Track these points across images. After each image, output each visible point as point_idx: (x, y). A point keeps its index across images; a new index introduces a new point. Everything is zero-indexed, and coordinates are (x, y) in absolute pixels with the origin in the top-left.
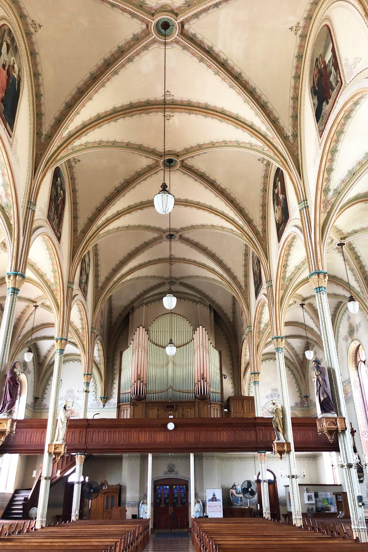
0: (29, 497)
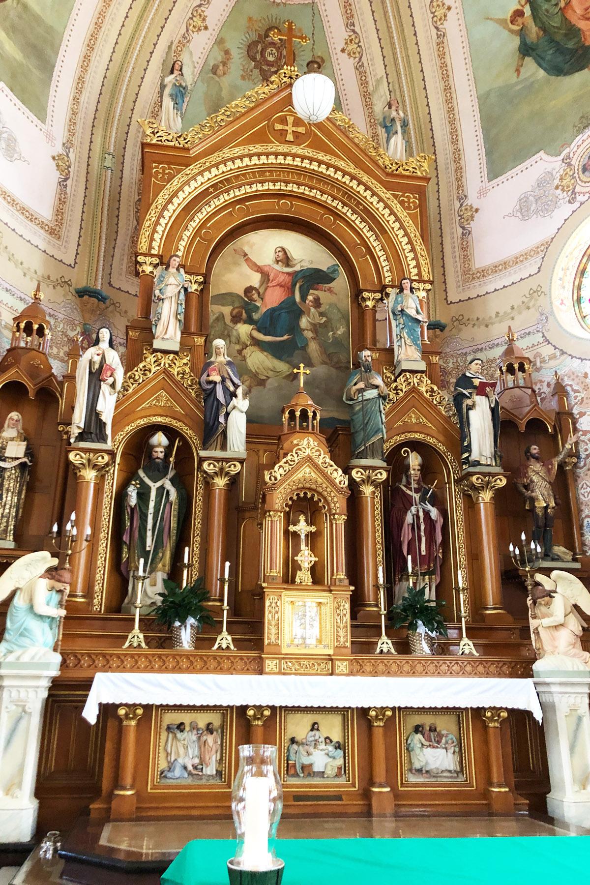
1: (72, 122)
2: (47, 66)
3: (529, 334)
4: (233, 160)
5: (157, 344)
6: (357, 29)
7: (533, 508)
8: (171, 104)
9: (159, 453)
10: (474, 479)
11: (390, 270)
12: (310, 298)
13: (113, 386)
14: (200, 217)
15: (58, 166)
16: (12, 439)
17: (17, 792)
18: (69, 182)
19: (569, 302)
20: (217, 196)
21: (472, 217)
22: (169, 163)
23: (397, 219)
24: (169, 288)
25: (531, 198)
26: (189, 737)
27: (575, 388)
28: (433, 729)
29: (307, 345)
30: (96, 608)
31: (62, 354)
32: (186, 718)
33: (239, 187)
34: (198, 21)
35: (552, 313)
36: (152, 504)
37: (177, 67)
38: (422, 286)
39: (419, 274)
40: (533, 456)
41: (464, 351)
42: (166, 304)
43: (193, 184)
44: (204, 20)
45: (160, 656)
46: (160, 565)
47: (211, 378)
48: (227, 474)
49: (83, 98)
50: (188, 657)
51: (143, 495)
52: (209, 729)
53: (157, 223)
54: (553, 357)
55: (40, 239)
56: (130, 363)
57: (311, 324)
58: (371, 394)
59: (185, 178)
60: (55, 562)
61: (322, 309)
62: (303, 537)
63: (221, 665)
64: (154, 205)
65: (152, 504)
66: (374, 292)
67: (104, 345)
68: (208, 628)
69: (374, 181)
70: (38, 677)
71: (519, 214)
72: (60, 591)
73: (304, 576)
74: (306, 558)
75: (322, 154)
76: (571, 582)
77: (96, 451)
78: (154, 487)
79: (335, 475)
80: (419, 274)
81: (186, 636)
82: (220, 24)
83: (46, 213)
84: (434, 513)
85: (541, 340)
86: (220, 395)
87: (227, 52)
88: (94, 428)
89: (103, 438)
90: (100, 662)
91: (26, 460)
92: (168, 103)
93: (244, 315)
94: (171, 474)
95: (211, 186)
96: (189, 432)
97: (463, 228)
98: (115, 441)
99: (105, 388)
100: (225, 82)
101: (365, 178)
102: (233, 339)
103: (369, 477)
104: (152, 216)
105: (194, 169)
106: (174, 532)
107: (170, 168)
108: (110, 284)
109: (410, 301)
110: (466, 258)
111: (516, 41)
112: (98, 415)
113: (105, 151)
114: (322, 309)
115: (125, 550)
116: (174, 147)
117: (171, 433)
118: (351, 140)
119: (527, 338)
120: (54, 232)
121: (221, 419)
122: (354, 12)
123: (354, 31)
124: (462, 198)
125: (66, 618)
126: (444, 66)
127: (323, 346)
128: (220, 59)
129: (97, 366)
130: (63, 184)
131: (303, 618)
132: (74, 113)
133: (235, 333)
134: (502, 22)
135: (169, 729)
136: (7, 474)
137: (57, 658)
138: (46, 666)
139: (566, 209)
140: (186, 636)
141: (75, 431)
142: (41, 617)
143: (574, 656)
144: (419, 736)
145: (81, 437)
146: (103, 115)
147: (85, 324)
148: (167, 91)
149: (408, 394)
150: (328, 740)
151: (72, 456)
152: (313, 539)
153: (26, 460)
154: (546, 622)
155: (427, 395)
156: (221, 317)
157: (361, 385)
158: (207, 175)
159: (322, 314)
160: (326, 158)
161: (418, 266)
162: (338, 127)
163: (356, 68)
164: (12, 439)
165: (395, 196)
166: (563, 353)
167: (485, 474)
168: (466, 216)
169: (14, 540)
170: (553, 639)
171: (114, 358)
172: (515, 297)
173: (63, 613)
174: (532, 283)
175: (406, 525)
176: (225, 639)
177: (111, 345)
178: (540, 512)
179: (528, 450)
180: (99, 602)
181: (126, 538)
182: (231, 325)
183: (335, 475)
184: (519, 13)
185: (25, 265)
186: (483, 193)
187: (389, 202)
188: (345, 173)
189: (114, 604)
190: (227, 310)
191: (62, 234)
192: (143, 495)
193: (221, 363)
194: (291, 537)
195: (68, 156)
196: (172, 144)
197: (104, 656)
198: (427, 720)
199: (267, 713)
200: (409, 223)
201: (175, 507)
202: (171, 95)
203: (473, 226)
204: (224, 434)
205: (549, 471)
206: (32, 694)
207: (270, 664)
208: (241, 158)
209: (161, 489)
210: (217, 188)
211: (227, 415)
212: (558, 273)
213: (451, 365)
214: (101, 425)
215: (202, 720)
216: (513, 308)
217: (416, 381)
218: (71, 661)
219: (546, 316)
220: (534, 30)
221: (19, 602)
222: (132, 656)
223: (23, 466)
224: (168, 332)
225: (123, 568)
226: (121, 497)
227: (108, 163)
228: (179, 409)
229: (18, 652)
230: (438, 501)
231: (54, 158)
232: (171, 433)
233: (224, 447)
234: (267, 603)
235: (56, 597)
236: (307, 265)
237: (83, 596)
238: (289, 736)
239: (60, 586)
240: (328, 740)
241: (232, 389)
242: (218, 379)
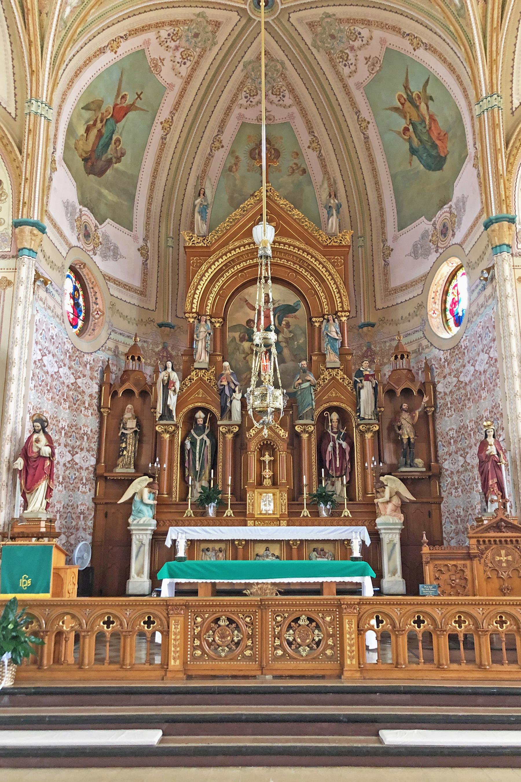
0: (408, 495)
1: (147, 224)
2: (132, 198)
3: (417, 331)
4: (234, 249)
5: (196, 365)
6: (316, 135)
7: (402, 439)
8: (199, 217)
9: (200, 422)
10: (361, 427)
11: (327, 304)
12: (284, 323)
13: (175, 391)
14: (220, 283)
15: (141, 253)
16: (129, 419)
17: (142, 576)
18: (148, 261)
19: (438, 312)
20: (227, 271)
21: (390, 254)
22: (199, 256)
23: (330, 274)
24: (201, 334)
25: (419, 246)
26: (211, 554)
27: (436, 366)
28: (322, 550)
29: (282, 351)
30: (174, 499)
31: (152, 362)
32: (210, 546)
33: (239, 264)
34: (217, 144)
35: (428, 320)
36: (198, 448)
37: (202, 192)
38: (343, 314)
39: (342, 307)
40: (403, 410)
41: (385, 340)
42: (200, 344)
43: (213, 267)
44: (221, 142)
45: (200, 520)
46: (203, 478)
47: (222, 383)
48: (232, 432)
49: (153, 208)
50: (212, 520)
51: (193, 443)
52: (220, 551)
53: (195, 293)
54: (427, 347)
55: (134, 299)
56: (183, 379)
57: (285, 338)
58: (306, 385)
59: (209, 265)
60: (151, 480)
61: (291, 329)
62: (267, 462)
63: (229, 523)
64: (192, 283)
65: (198, 448)
66: (319, 317)
67: (170, 370)
68: (222, 506)
69: (316, 252)
70: (147, 530)
71: (413, 255)
72: (153, 493)
73: (267, 482)
74: (267, 473)
75: (286, 238)
76: (394, 480)
77: (168, 425)
78: (199, 439)
79: (280, 432)
80: (342, 307)
81: (211, 511)
82: (231, 143)
83: (137, 283)
84: (344, 445)
85: (422, 336)
86: (227, 392)
87: (237, 158)
88: (167, 413)
89: (171, 418)
90: (174, 523)
91: (137, 429)
92: (197, 217)
93: (247, 336)
94: (207, 432)
95: (224, 266)
96: (215, 410)
97: (385, 261)
98: (177, 419)
99: (171, 392)
100: (238, 175)
101: (311, 250)
102: (241, 351)
103: (304, 429)
104: (191, 291)
105: (211, 260)
106: (209, 461)
107: (200, 259)
108: (177, 316)
109: (332, 327)
110: (387, 281)
111: (407, 146)
112: (168, 406)
113: (167, 237)
114: (291, 329)
115: (187, 470)
116: (202, 247)
117: (206, 411)
118: (303, 227)
119: (416, 334)
120: (142, 293)
121: (228, 404)
122: (313, 125)
123: (314, 136)
124: (384, 241)
125: (157, 504)
126: (370, 155)
127: (291, 351)
128: (233, 162)
129: (166, 382)
130: (145, 264)
131: (266, 502)
132: (148, 218)
133: (242, 348)
134: (399, 133)
135: (203, 550)
136: (129, 436)
137: (155, 522)
138: (150, 525)
139: (433, 257)
140: (211, 511)
141: (158, 415)
142: (147, 505)
143: (394, 516)
144: (315, 553)
145: (161, 418)
146: (164, 214)
147: (164, 343)
148: (197, 209)
149: (330, 381)
150: (273, 555)
151: (157, 428)
152: (273, 463)
153: (137, 429)
154: (380, 500)
155: (341, 381)
156: (234, 339)
157: (300, 381)
158: (221, 260)
159: (290, 332)
160: (288, 241)
161: (341, 302)
162: (295, 220)
163: (318, 157)
164: (129, 419)
165: (329, 260)
166: (432, 345)
167: (366, 424)
168: (387, 252)
169: (134, 468)
170: (386, 508)
171: (174, 376)
172: (410, 308)
173: (156, 502)
174: (417, 300)
175: (328, 452)
176: (229, 512)
177: (173, 369)
178: (405, 441)
179: (401, 407)
180: (176, 496)
181: (186, 465)
182: (239, 343)
183: (280, 432)
184: (406, 129)
185: (129, 317)
186: (395, 238)
187: (325, 264)
188: (299, 249)
189: (183, 497)
190: (237, 335)
191: (147, 293)
192: (193, 443)
193: (227, 375)
194: (261, 463)
195: (147, 246)
196: (200, 245)
197: (175, 521)
198: (320, 546)
199: (243, 543)
200: (336, 276)
201: (209, 448)
202: (199, 212)
203: (390, 260)
204: (230, 411)
205: (413, 418)
206: (144, 537)
207: (250, 522)
208: (239, 247)
209: (203, 439)
210: (227, 266)
211: (231, 401)
212: (431, 294)
213: (378, 349)
214: (170, 411)
215: (217, 546)
216: (409, 314)
217: (335, 373)
218: (161, 523)
219: (425, 321)
220: (416, 142)
221: (137, 498)
222: (188, 520)
223: (135, 432)
224: (202, 358)
225: (186, 479)
226: (183, 445)
227: (170, 244)
228: (209, 398)
229: (138, 520)
230: (348, 437)
231: (139, 250)
232: (206, 411)
233: (230, 418)
234: (248, 495)
235: (152, 496)
236: (282, 303)
237: (167, 494)
238: (256, 553)
239: (154, 491)
240: (273, 555)
241: (233, 387)
242: (225, 383)
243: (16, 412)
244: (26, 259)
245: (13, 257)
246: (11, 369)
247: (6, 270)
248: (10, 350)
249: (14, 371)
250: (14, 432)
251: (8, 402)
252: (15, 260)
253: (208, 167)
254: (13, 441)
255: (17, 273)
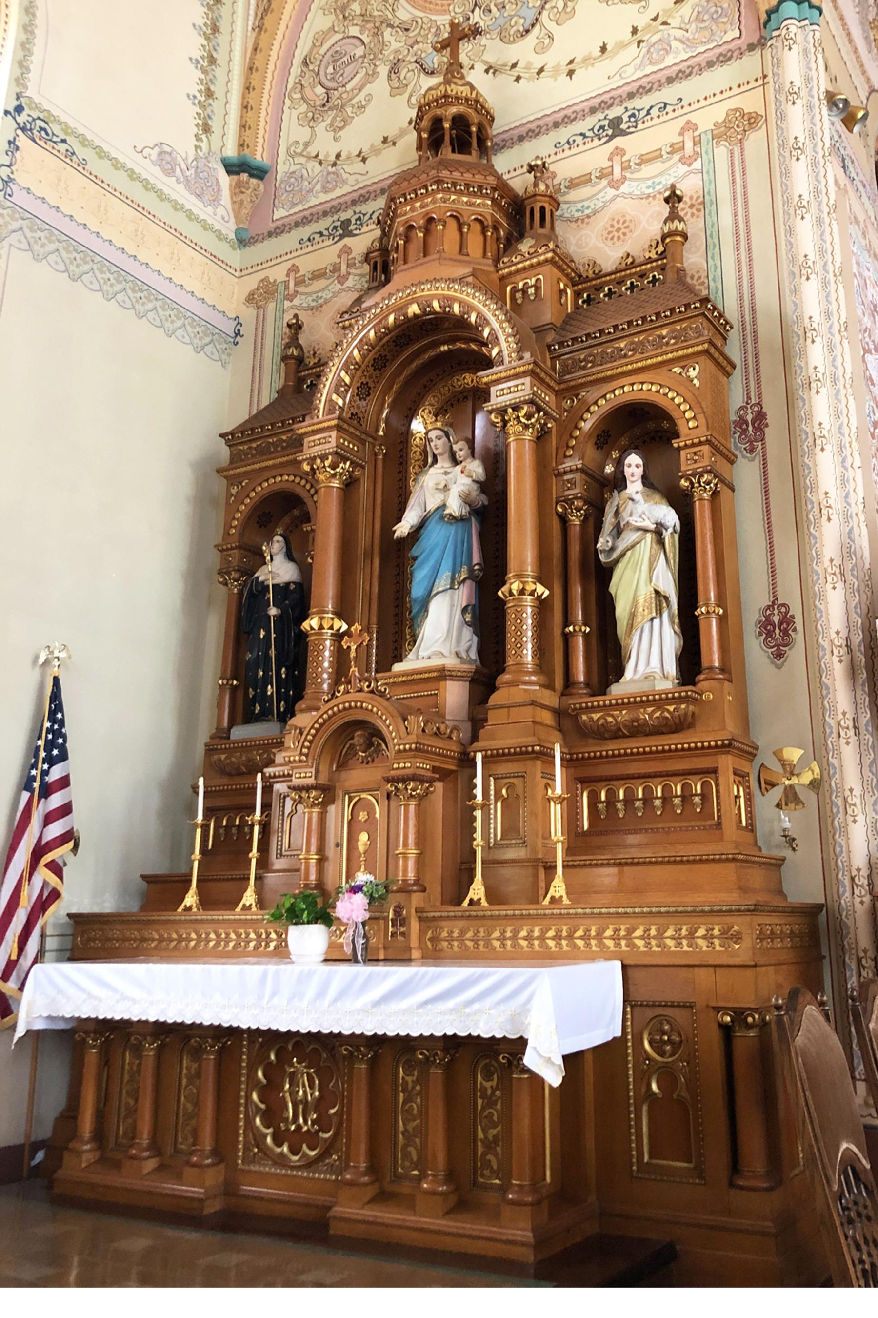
243: (844, 481)
244: (793, 29)
245: (751, 47)
246: (803, 353)
247: (736, 90)
248: (789, 308)
249: (816, 356)
250: (848, 550)
251: (811, 454)
252: (757, 53)
253: (838, 474)
254: (849, 577)
255: (770, 88)
